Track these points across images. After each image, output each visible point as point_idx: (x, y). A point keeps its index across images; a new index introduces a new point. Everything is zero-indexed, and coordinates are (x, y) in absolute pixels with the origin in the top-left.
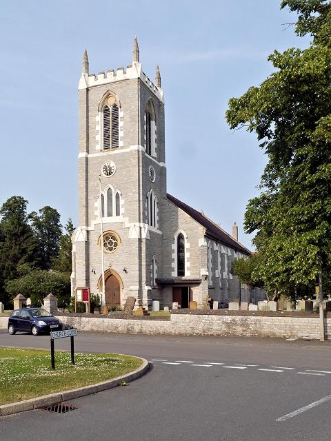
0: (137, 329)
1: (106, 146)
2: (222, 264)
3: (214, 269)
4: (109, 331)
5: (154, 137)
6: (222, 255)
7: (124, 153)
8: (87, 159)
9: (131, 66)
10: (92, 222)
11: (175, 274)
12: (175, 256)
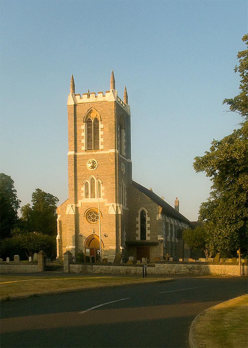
0: (133, 272)
1: (89, 148)
2: (171, 231)
3: (166, 236)
4: (113, 273)
5: (124, 141)
6: (171, 225)
7: (104, 154)
8: (75, 156)
9: (109, 92)
10: (80, 202)
11: (138, 239)
12: (138, 226)
